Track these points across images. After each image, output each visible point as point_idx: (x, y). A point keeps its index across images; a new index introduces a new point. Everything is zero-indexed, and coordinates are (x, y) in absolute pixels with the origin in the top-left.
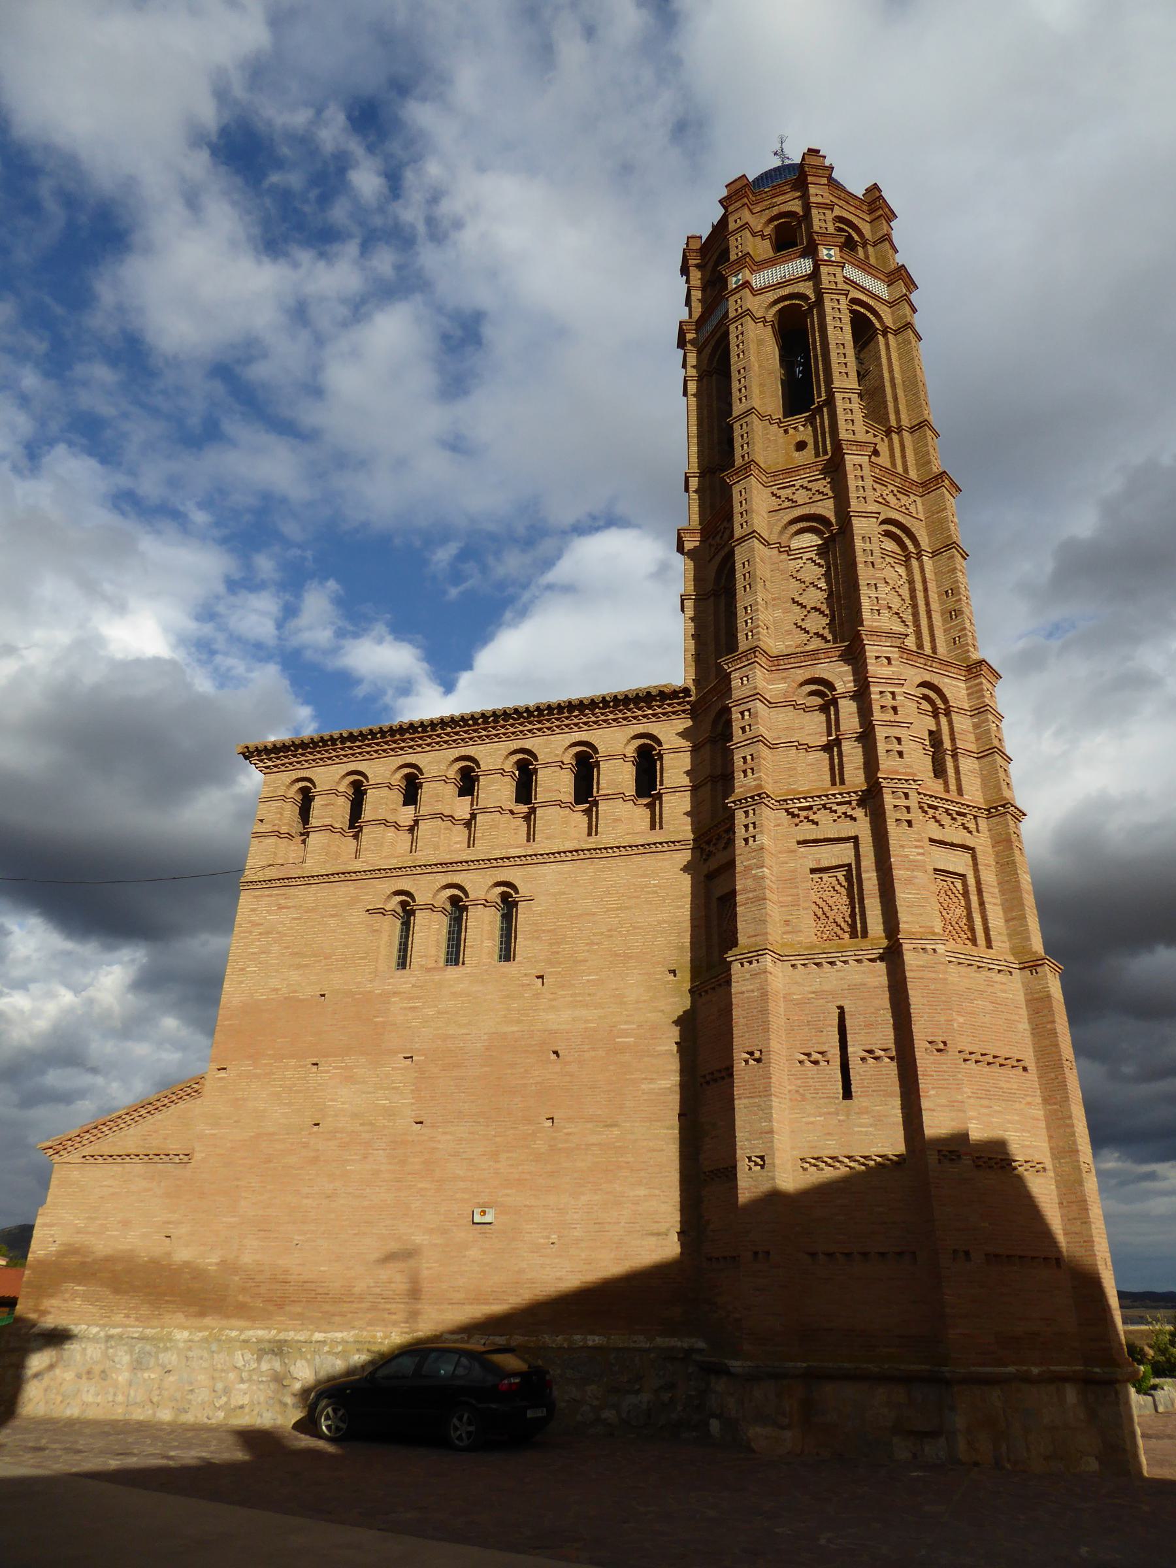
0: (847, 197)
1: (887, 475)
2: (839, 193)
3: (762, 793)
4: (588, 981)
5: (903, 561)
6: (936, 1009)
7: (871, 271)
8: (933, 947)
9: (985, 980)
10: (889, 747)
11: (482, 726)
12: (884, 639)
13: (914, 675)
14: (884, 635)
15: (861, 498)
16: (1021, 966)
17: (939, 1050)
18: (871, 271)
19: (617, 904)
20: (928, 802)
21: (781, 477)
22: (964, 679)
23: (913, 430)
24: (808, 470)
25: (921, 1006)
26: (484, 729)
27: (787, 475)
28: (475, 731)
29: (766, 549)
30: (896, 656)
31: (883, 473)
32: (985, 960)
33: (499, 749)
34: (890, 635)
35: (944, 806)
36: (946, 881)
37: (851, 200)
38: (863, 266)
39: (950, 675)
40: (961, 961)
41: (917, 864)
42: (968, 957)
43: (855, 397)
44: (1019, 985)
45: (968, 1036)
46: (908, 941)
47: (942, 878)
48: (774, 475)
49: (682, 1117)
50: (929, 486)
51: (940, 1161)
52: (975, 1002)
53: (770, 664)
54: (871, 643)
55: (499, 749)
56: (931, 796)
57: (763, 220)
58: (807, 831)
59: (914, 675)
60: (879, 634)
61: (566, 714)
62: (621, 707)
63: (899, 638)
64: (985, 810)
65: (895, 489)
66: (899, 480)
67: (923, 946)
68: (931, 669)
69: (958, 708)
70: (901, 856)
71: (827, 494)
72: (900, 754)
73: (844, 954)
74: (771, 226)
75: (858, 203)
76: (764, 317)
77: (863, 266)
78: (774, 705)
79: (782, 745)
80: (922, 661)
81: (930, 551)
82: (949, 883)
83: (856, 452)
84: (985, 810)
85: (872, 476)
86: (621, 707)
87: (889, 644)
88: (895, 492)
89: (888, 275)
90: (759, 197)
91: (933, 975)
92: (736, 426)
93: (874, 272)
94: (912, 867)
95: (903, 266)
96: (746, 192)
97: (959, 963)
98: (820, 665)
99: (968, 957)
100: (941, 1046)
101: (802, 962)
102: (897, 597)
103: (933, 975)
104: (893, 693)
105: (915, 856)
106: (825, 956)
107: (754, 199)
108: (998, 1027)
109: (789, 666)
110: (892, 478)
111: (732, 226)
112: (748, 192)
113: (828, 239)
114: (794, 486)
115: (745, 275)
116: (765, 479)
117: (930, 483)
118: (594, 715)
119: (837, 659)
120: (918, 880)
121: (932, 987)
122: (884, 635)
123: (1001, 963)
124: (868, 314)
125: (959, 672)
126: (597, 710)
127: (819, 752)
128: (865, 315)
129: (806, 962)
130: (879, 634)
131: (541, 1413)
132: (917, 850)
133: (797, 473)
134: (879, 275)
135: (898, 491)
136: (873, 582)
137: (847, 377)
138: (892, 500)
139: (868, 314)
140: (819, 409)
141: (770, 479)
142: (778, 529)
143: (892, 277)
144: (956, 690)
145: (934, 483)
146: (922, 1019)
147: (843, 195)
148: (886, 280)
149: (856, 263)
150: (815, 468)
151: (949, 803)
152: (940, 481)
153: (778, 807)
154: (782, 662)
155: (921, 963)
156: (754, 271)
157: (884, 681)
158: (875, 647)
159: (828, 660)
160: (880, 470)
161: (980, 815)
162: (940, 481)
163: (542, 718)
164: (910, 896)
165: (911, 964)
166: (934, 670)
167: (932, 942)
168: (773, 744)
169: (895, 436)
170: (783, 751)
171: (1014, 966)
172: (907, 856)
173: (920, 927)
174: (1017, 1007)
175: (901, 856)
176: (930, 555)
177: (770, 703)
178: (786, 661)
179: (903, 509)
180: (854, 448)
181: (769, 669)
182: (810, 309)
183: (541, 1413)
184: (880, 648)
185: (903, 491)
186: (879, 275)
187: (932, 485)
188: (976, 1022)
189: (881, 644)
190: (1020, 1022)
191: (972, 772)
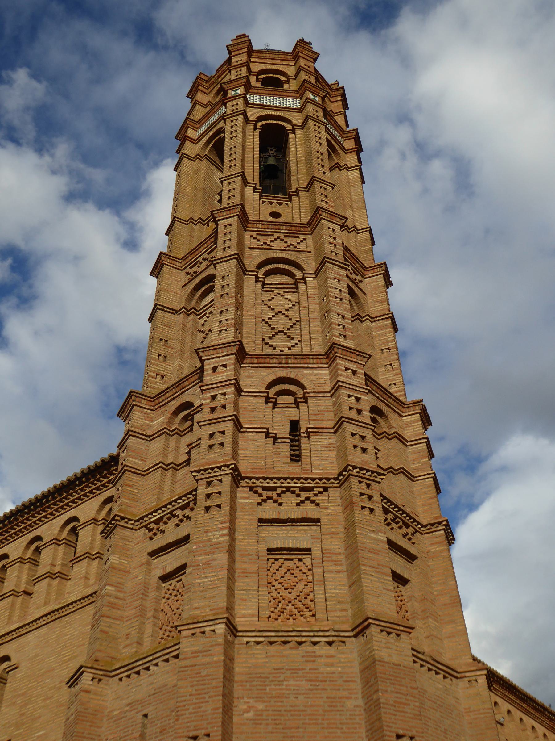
0: (271, 55)
1: (270, 227)
2: (264, 55)
4: (38, 737)
5: (294, 288)
6: (204, 698)
7: (281, 94)
8: (212, 628)
9: (303, 657)
11: (9, 526)
12: (220, 350)
14: (219, 347)
16: (354, 632)
18: (281, 94)
19: (69, 655)
20: (261, 485)
21: (190, 258)
22: (327, 366)
24: (206, 245)
25: (188, 698)
26: (12, 528)
27: (193, 255)
28: (7, 532)
29: (176, 315)
31: (266, 226)
32: (304, 634)
33: (22, 542)
34: (225, 346)
35: (283, 485)
36: (292, 560)
37: (276, 56)
38: (273, 93)
39: (310, 366)
40: (272, 639)
41: (219, 545)
42: (280, 634)
44: (355, 655)
45: (267, 724)
46: (186, 627)
47: (285, 557)
48: (184, 258)
50: (313, 223)
52: (285, 683)
53: (153, 404)
54: (209, 357)
55: (22, 542)
56: (265, 479)
57: (212, 94)
60: (214, 348)
61: (59, 498)
62: (92, 480)
63: (234, 346)
64: (334, 479)
65: (282, 236)
66: (284, 228)
67: (202, 629)
68: (287, 366)
69: (314, 392)
70: (204, 542)
73: (155, 656)
75: (283, 56)
77: (273, 93)
78: (152, 438)
79: (151, 470)
80: (275, 361)
81: (313, 272)
82: (296, 561)
83: (227, 216)
84: (334, 479)
86: (92, 480)
87: (225, 354)
88: (255, 236)
89: (297, 92)
90: (210, 82)
91: (207, 659)
93: (285, 94)
94: (213, 550)
95: (343, 88)
96: (199, 82)
97: (271, 643)
98: (187, 392)
99: (280, 634)
101: (126, 674)
102: (285, 318)
103: (207, 659)
105: (218, 538)
106: (140, 662)
107: (208, 85)
108: (316, 708)
109: (166, 401)
110: (277, 227)
112: (201, 82)
113: (234, 83)
114: (199, 261)
116: (179, 264)
117: (313, 221)
118: (76, 492)
119: (197, 381)
120: (217, 562)
121: (204, 673)
122: (219, 347)
123: (327, 634)
124: (281, 123)
125: (319, 361)
126: (77, 488)
127: (186, 468)
128: (278, 124)
129: (129, 673)
130: (214, 348)
132: (221, 532)
133: (199, 251)
134: (290, 94)
136: (224, 309)
139: (281, 123)
141: (183, 263)
143: (301, 92)
145: (315, 219)
146: (187, 712)
147: (268, 55)
148: (298, 95)
149: (267, 92)
150: (209, 242)
151: (289, 481)
152: (318, 215)
153: (139, 526)
154: (161, 400)
155: (195, 649)
156: (197, 128)
157: (215, 385)
158: (213, 360)
159: (191, 385)
160: (263, 224)
161: (331, 485)
162: (318, 215)
163: (44, 507)
164: (206, 580)
165: (186, 652)
166: (291, 366)
167: (211, 623)
168: (145, 471)
170: (153, 474)
171: (347, 634)
172: (210, 540)
173: (211, 610)
174: (347, 681)
175: (204, 542)
176: (314, 276)
177: (149, 436)
178: (163, 398)
179: (265, 246)
180: (225, 213)
181: (153, 408)
184: (217, 359)
185: (291, 235)
186: (290, 94)
187: (315, 222)
188: (282, 706)
189: (218, 355)
190: (351, 698)
191: (326, 447)
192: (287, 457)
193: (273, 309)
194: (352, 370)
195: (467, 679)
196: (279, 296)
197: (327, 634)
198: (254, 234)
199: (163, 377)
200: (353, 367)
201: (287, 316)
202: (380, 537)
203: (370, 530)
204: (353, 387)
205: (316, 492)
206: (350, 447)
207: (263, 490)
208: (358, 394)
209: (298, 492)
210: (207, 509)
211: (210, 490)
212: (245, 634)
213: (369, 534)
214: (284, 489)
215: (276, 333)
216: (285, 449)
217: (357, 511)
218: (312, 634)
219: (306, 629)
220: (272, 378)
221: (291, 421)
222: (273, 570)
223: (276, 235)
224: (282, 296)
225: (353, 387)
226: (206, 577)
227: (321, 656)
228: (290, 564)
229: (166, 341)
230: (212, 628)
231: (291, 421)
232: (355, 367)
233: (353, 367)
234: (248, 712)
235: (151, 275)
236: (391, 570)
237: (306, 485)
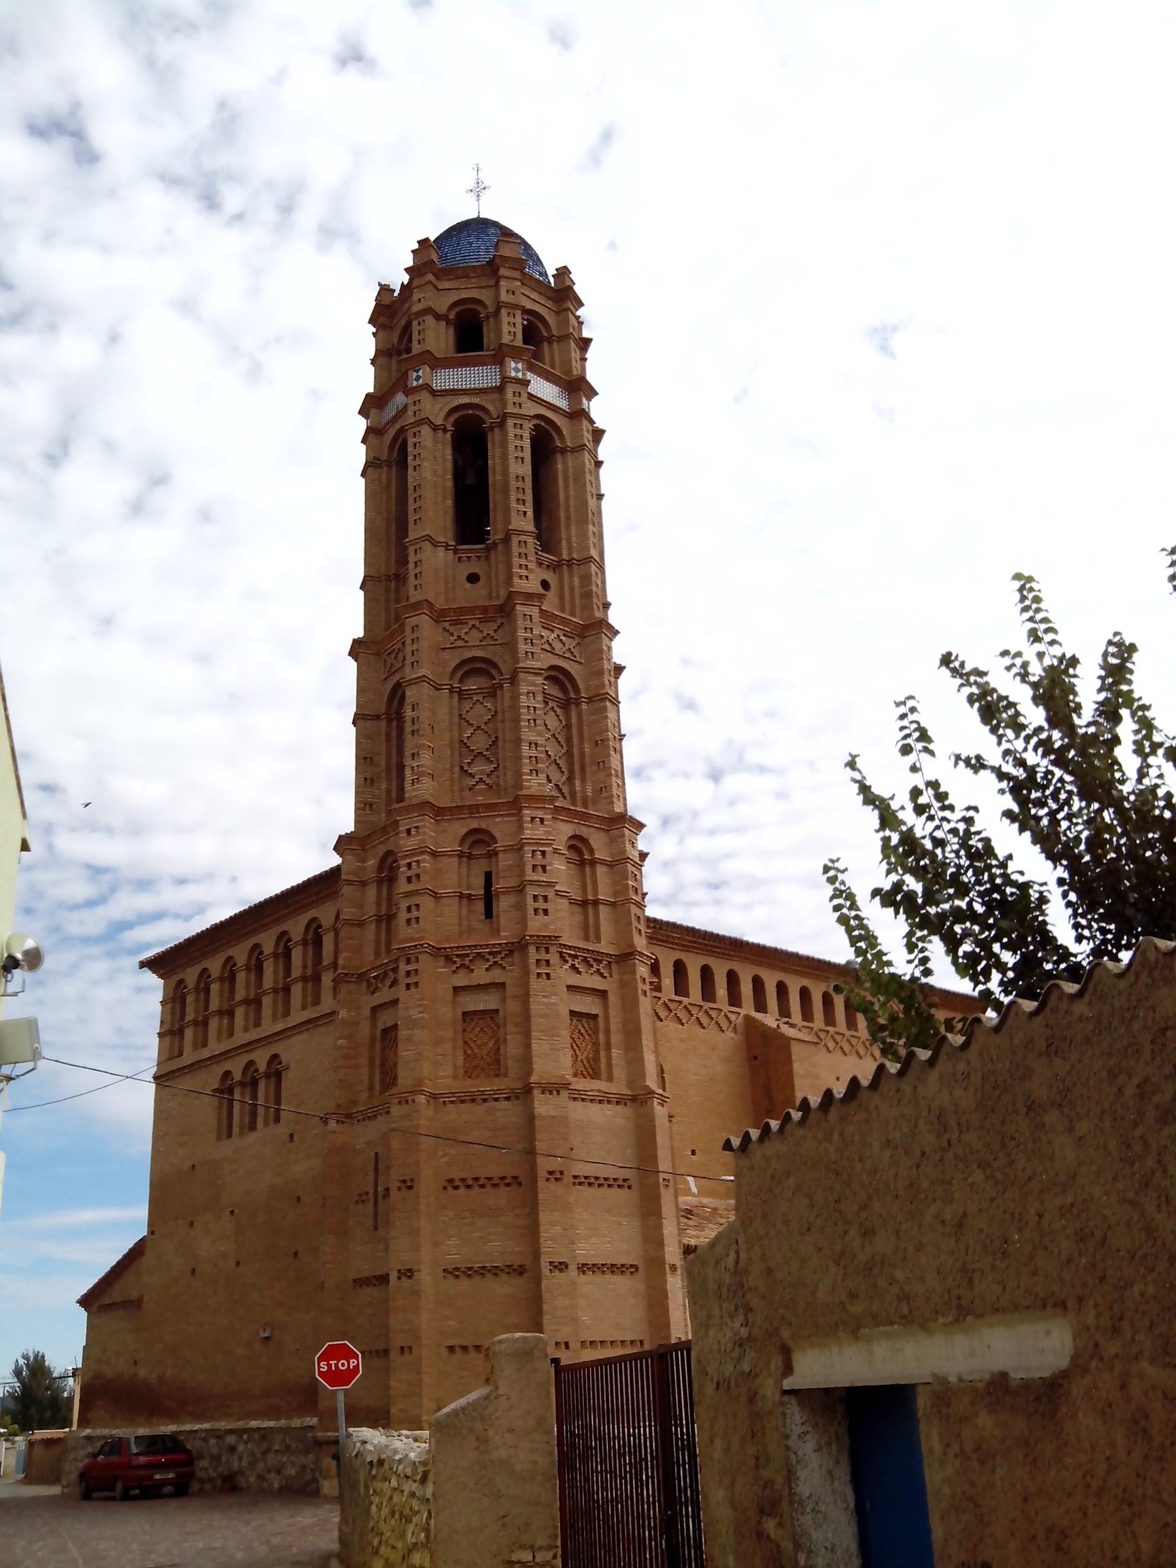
8: (412, 1098)
10: (537, 905)
13: (565, 830)
17: (557, 1179)
30: (550, 817)
40: (462, 1099)
42: (468, 1094)
49: (167, 1039)
51: (399, 1278)
58: (461, 980)
59: (565, 830)
65: (561, 633)
71: (496, 640)
72: (546, 912)
74: (452, 419)
92: (411, 550)
99: (468, 1094)
100: (558, 1175)
104: (543, 853)
131: (983, 980)
135: (564, 635)
137: (523, 463)
138: (557, 646)
142: (442, 415)
182: (487, 318)
183: (983, 980)
192: (413, 1024)
194: (540, 818)
195: (640, 1101)
196: (478, 706)
197: (505, 1092)
200: (540, 814)
201: (486, 732)
202: (552, 1001)
204: (538, 841)
206: (531, 912)
209: (487, 957)
210: (408, 986)
211: (409, 968)
216: (480, 906)
217: (533, 977)
218: (492, 1092)
219: (488, 1089)
220: (465, 830)
221: (486, 873)
223: (471, 623)
224: (482, 703)
225: (538, 841)
227: (499, 1110)
228: (481, 1023)
229: (371, 758)
231: (486, 873)
232: (542, 813)
233: (540, 814)
234: (444, 1157)
236: (1027, 620)
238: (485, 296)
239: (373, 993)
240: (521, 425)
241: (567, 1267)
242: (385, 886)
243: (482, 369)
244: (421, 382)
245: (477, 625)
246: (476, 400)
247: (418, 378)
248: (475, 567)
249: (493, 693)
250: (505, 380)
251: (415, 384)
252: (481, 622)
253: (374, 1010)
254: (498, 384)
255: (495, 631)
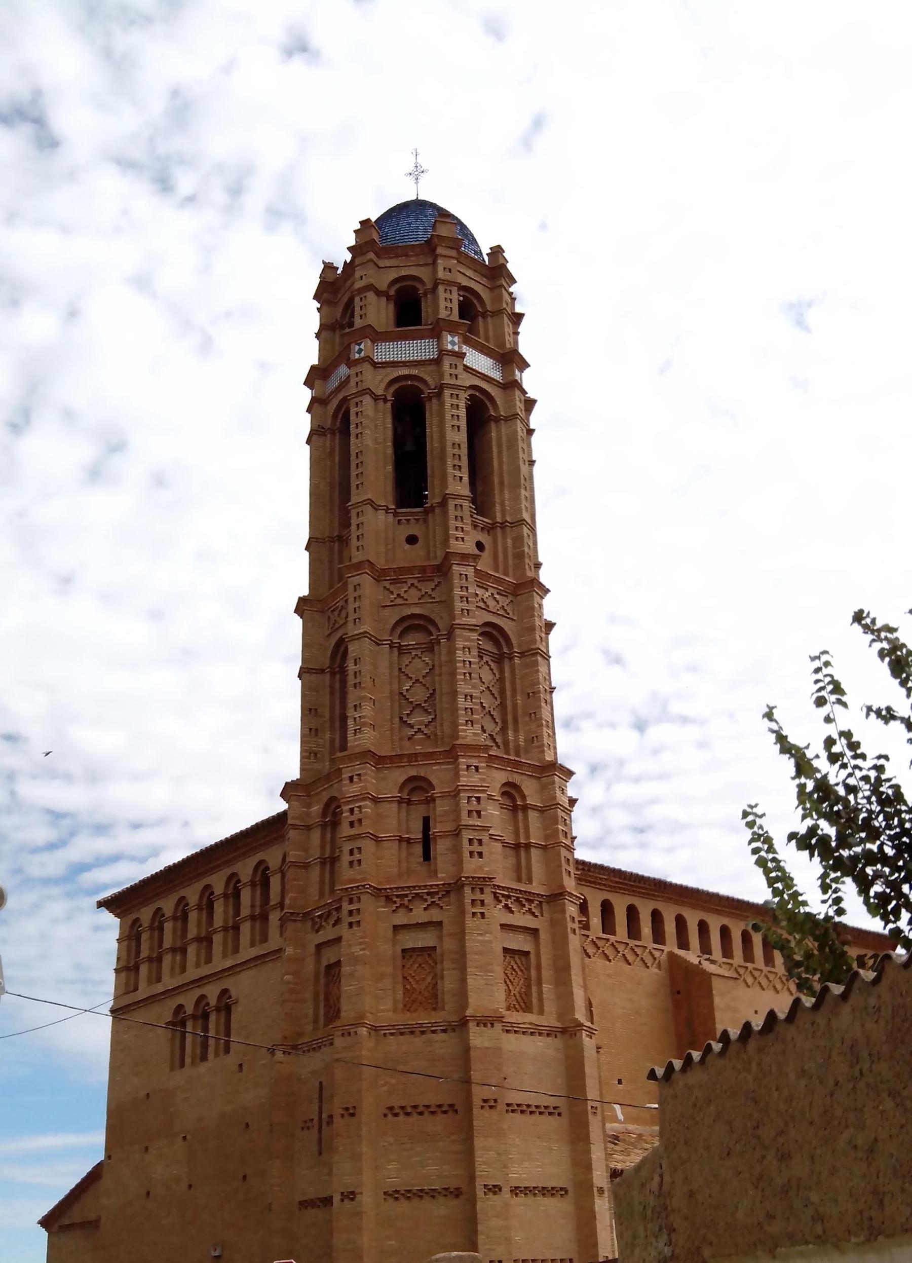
3: (365, 885)
8: (355, 1030)
10: (472, 848)
13: (499, 777)
15: (464, 588)
17: (491, 1107)
23: (522, 655)
43: (466, 504)
58: (401, 918)
59: (499, 777)
65: (495, 592)
68: (417, 763)
72: (480, 855)
76: (385, 395)
85: (475, 580)
104: (478, 799)
111: (356, 263)
114: (338, 607)
115: (365, 345)
135: (498, 593)
137: (459, 431)
138: (491, 603)
139: (475, 301)
140: (432, 509)
142: (383, 386)
144: (529, 787)
158: (350, 768)
166: (420, 763)
169: (520, 814)
182: (425, 294)
193: (411, 678)
198: (387, 584)
199: (316, 754)
200: (475, 762)
201: (424, 685)
202: (487, 939)
203: (477, 934)
204: (473, 788)
205: (440, 896)
206: (466, 854)
207: (397, 898)
208: (477, 793)
211: (352, 907)
212: (381, 1028)
213: (477, 938)
214: (413, 895)
215: (414, 708)
217: (468, 917)
222: (408, 966)
223: (410, 582)
224: (420, 658)
225: (473, 788)
226: (350, 986)
229: (316, 710)
230: (355, 1030)
232: (477, 761)
233: (475, 762)
235: (354, 231)
237: (432, 890)
238: (423, 273)
239: (317, 931)
240: (457, 395)
241: (500, 1190)
242: (329, 829)
243: (413, 343)
244: (362, 354)
245: (416, 584)
246: (414, 372)
247: (360, 351)
248: (414, 530)
249: (430, 648)
250: (442, 352)
251: (357, 356)
252: (419, 581)
253: (319, 947)
254: (436, 357)
255: (433, 590)
